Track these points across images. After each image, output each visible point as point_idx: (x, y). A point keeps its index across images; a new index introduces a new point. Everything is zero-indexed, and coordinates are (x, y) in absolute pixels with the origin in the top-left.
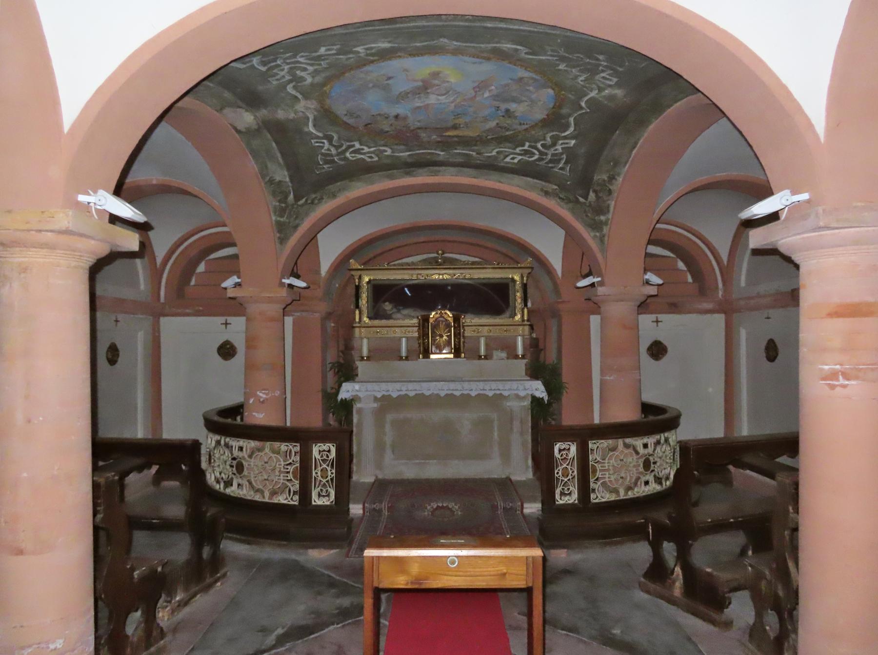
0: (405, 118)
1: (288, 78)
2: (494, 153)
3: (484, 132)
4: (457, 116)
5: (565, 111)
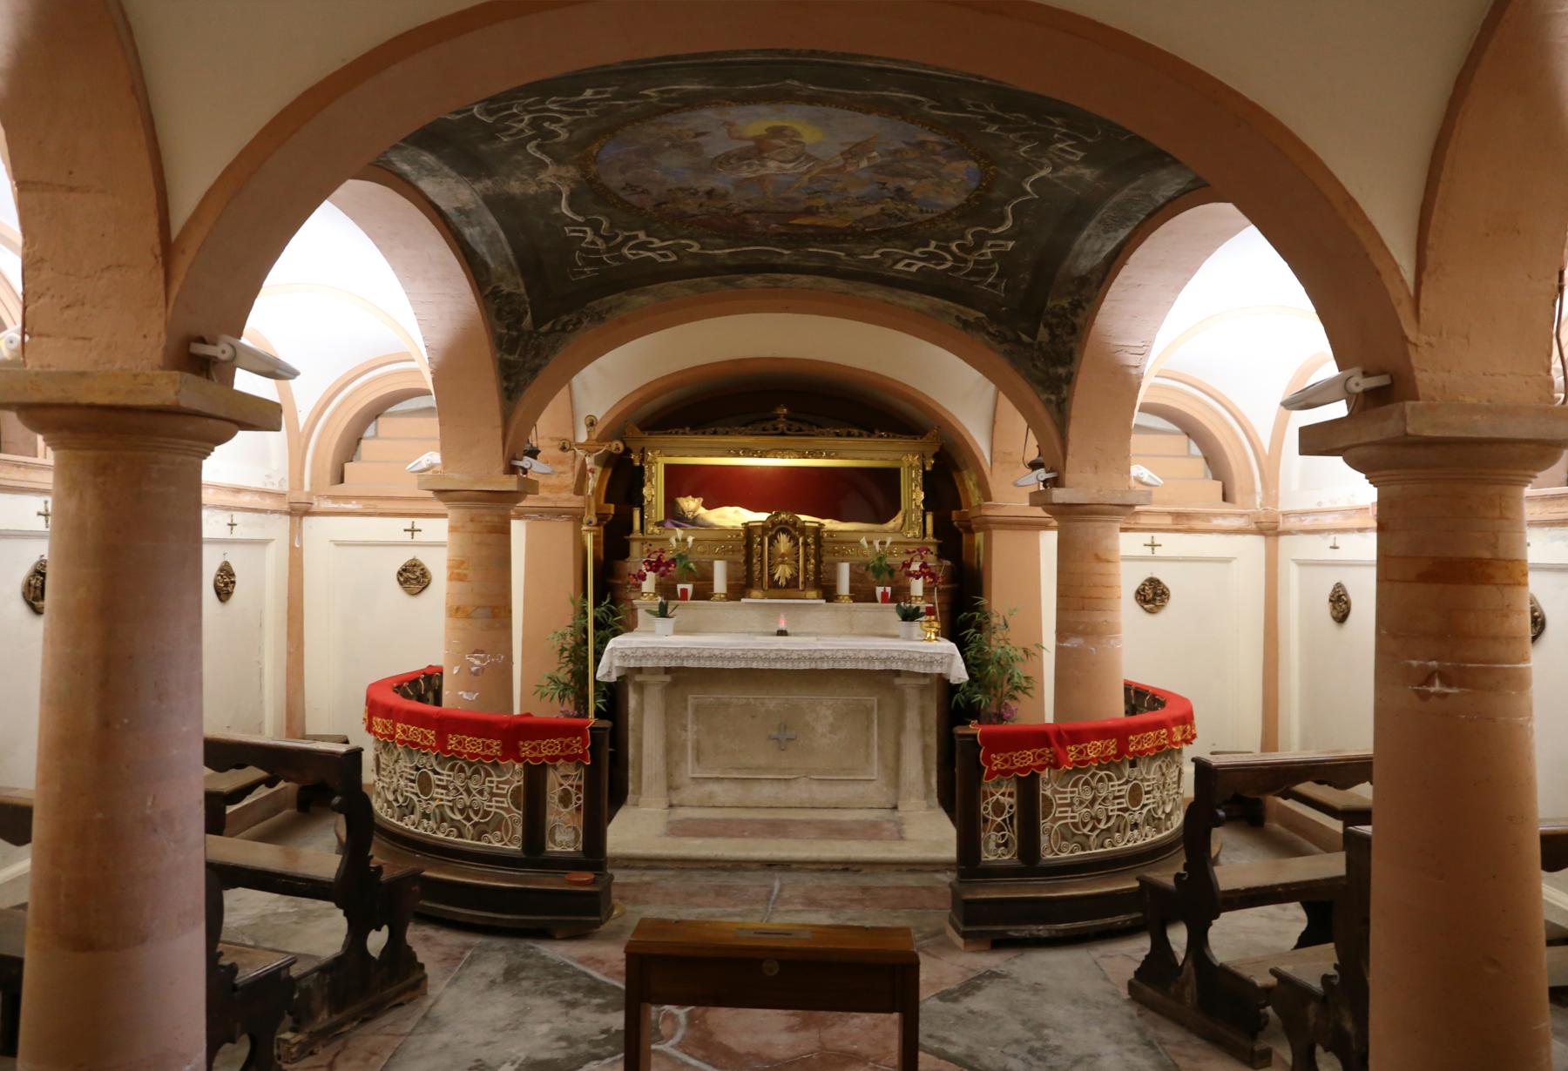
0: (724, 196)
1: (528, 132)
2: (876, 256)
3: (860, 221)
4: (813, 194)
5: (998, 194)
